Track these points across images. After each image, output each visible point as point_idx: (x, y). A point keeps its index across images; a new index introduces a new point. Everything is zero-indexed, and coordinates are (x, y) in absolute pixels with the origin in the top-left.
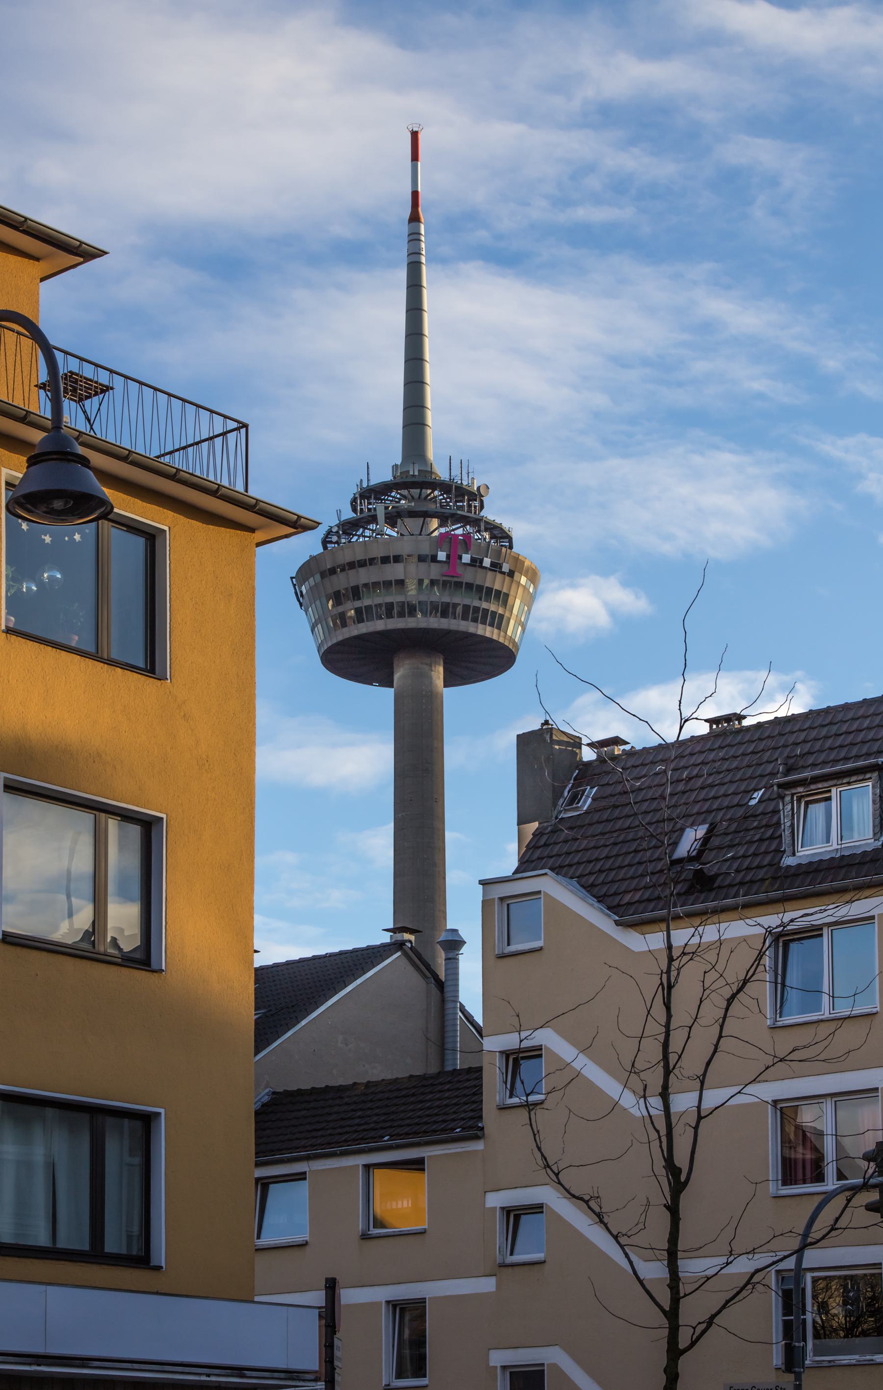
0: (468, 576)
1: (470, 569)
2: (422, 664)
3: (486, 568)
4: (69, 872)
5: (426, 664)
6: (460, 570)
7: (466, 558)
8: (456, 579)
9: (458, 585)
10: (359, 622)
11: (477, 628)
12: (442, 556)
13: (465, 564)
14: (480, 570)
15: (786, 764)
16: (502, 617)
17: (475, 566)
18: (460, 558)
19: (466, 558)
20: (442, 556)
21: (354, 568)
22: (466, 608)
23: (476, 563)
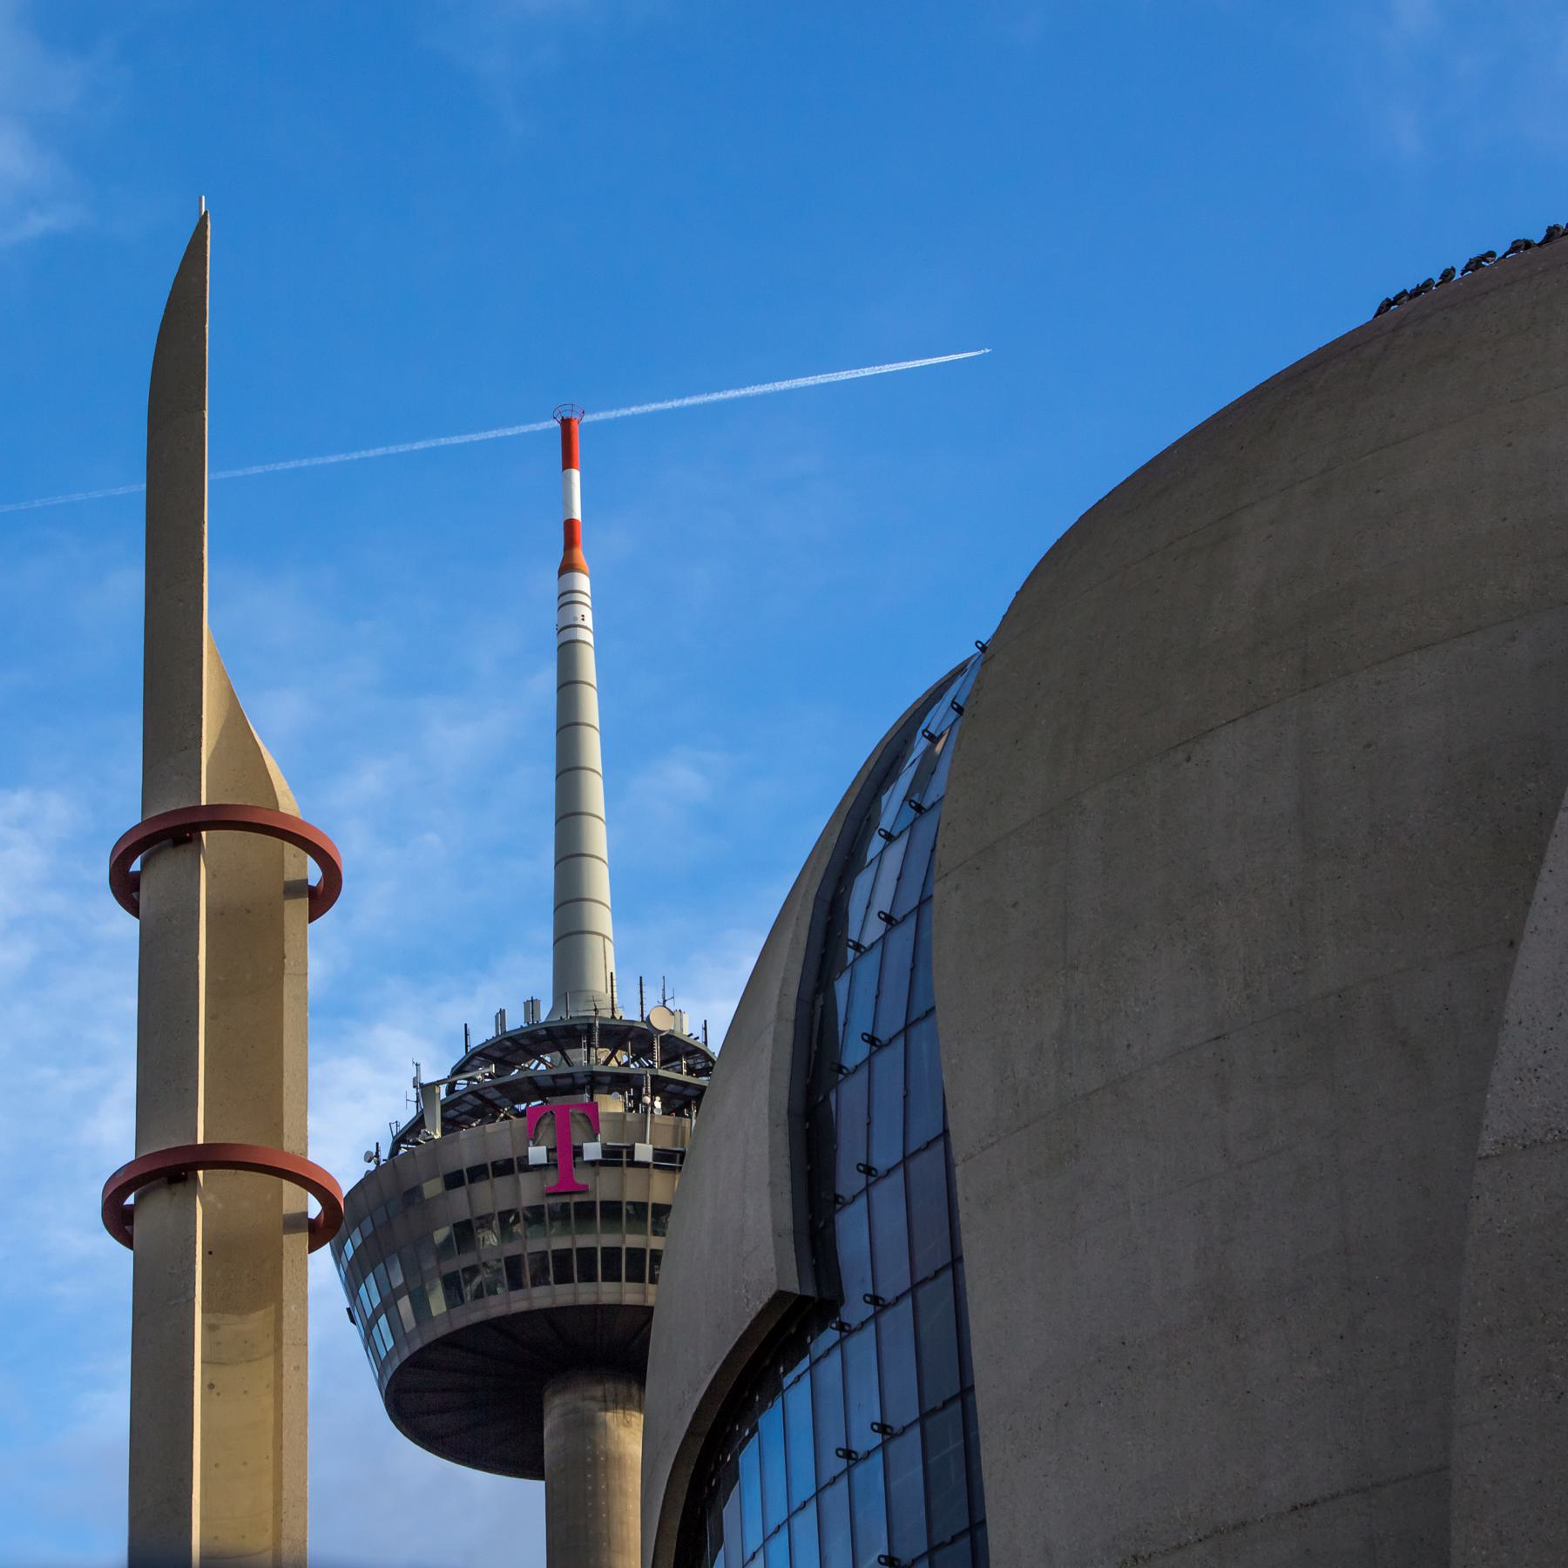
0: (604, 1187)
1: (607, 1174)
2: (584, 1399)
3: (645, 1165)
4: (583, 932)
5: (594, 1399)
6: (581, 1177)
7: (592, 1151)
8: (577, 1198)
9: (585, 1212)
10: (468, 1223)
11: (644, 1293)
12: (537, 1154)
13: (593, 1163)
14: (631, 1171)
15: (841, 1327)
16: (656, 1256)
17: (620, 1164)
18: (578, 1152)
19: (592, 1151)
20: (537, 1154)
21: (462, 1183)
22: (612, 1254)
23: (616, 1157)
